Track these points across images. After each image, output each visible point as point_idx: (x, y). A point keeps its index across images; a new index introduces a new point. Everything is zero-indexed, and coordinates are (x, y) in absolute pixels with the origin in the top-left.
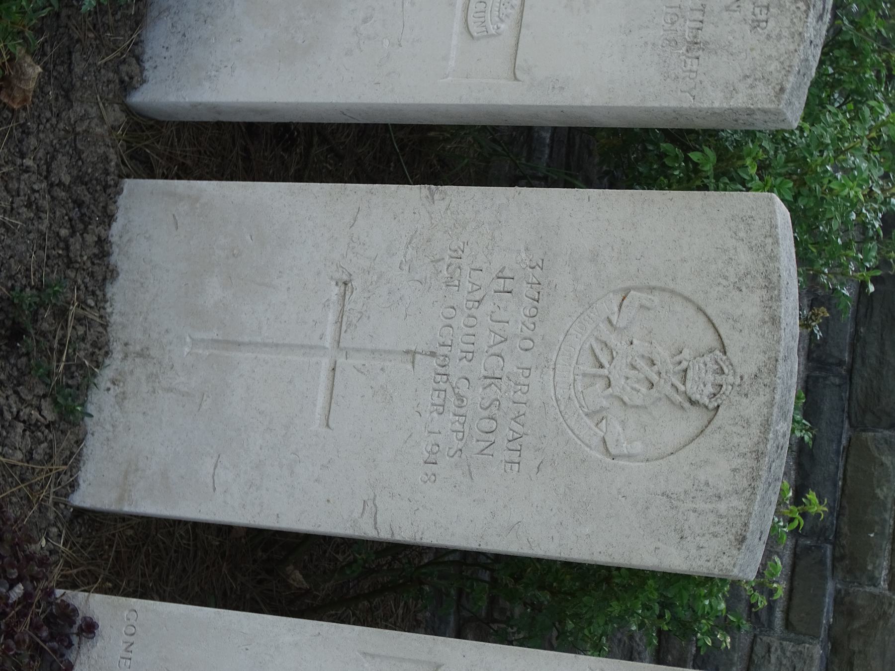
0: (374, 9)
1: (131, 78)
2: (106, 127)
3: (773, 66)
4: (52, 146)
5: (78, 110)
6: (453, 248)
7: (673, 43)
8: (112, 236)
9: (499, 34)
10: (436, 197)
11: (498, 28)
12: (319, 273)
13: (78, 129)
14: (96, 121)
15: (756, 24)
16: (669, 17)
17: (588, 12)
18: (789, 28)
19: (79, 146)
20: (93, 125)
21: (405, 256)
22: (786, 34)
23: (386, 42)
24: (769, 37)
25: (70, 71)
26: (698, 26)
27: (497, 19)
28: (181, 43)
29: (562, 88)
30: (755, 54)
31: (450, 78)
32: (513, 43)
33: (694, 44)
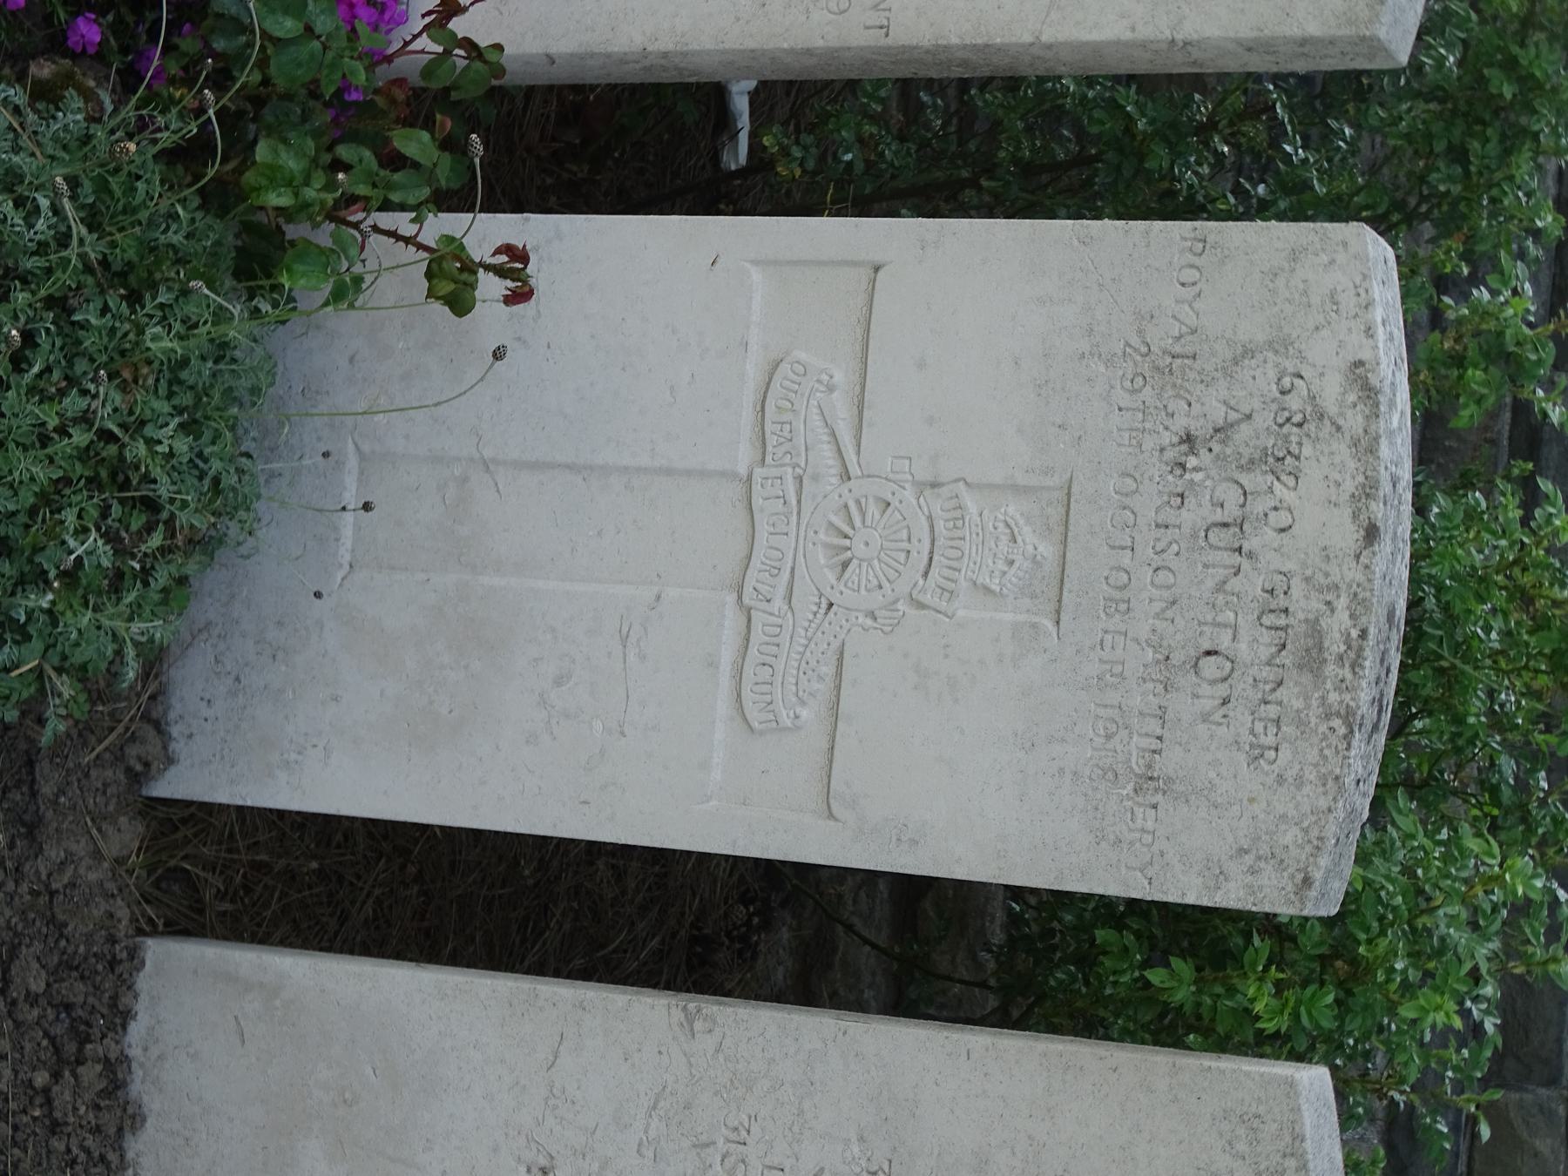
0: (574, 661)
1: (147, 765)
2: (106, 865)
3: (1290, 836)
4: (9, 928)
5: (53, 854)
6: (730, 1124)
7: (1110, 775)
8: (130, 1046)
9: (798, 728)
10: (698, 1025)
11: (797, 717)
12: (496, 1150)
13: (54, 886)
14: (88, 861)
15: (1257, 754)
16: (1100, 724)
17: (956, 701)
18: (1316, 765)
19: (61, 917)
20: (82, 871)
21: (646, 1132)
22: (1312, 777)
23: (598, 725)
24: (1280, 779)
25: (34, 794)
26: (1153, 747)
27: (794, 699)
28: (233, 694)
29: (914, 842)
30: (1257, 809)
31: (714, 803)
32: (825, 745)
33: (1148, 780)
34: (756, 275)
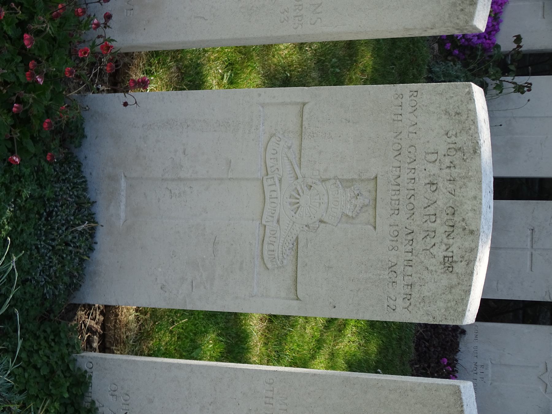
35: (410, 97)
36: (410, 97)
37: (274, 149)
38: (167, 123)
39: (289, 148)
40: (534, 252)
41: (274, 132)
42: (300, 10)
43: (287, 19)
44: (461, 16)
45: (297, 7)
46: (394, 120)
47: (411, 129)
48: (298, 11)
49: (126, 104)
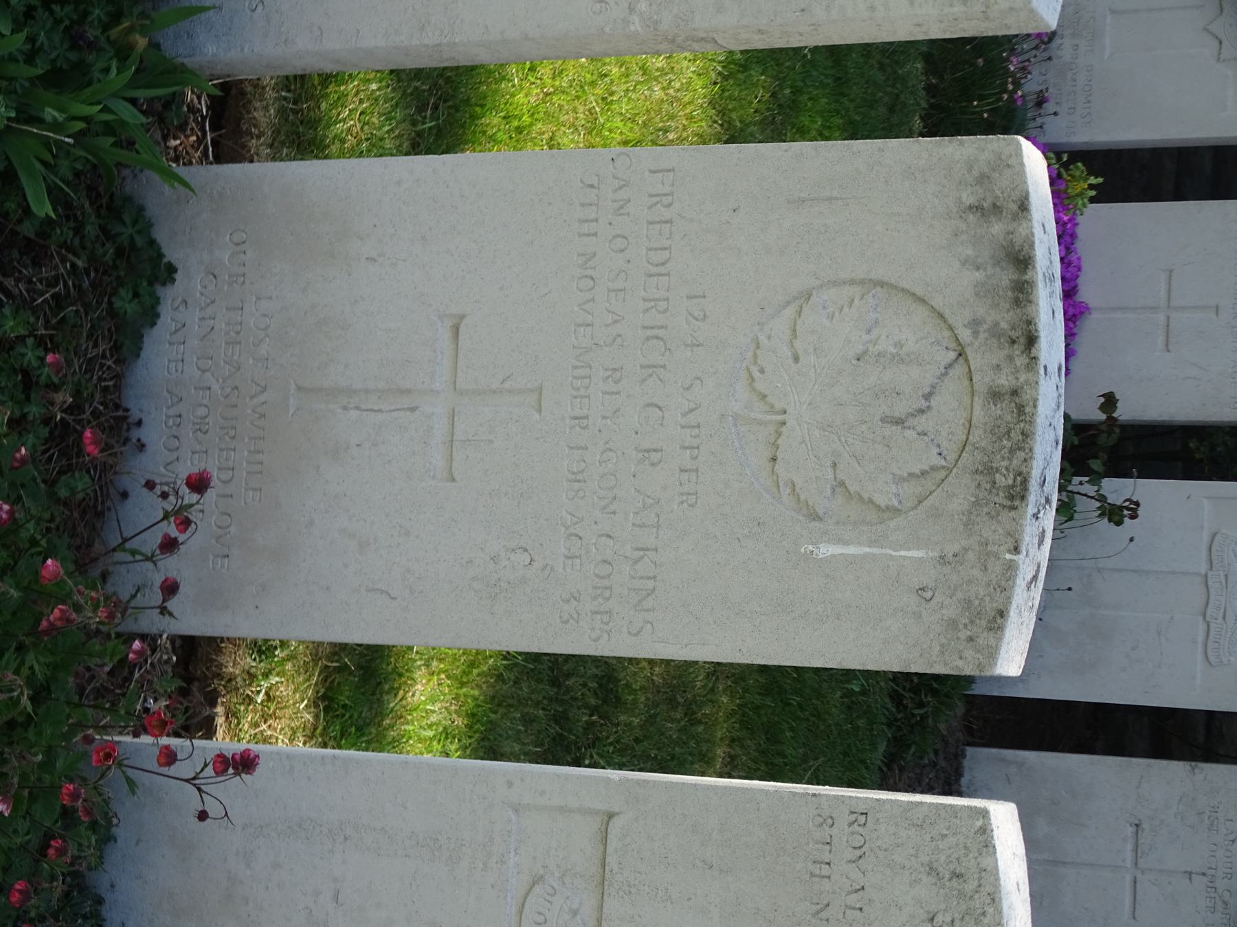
34: (1205, 502)
35: (850, 824)
36: (850, 824)
37: (540, 913)
38: (300, 826)
39: (575, 913)
40: (1139, 876)
41: (542, 872)
42: (608, 599)
43: (575, 616)
44: (968, 653)
45: (599, 592)
46: (812, 875)
47: (852, 900)
48: (600, 600)
49: (203, 816)
